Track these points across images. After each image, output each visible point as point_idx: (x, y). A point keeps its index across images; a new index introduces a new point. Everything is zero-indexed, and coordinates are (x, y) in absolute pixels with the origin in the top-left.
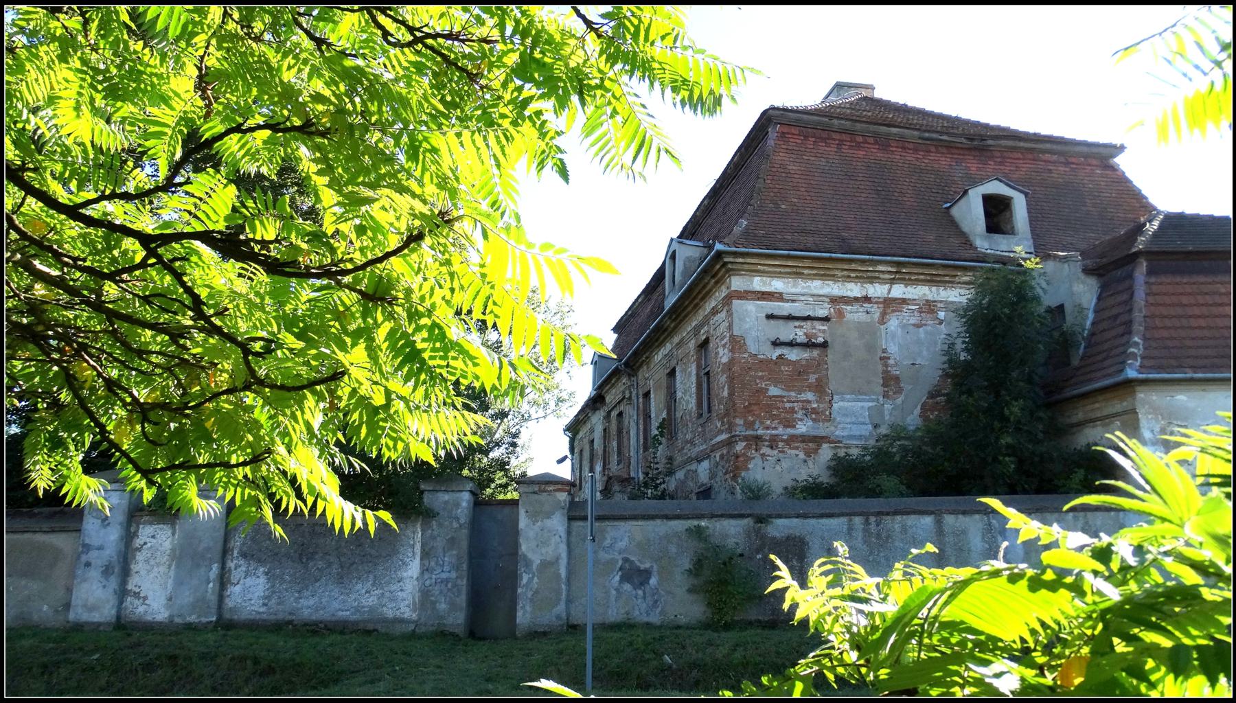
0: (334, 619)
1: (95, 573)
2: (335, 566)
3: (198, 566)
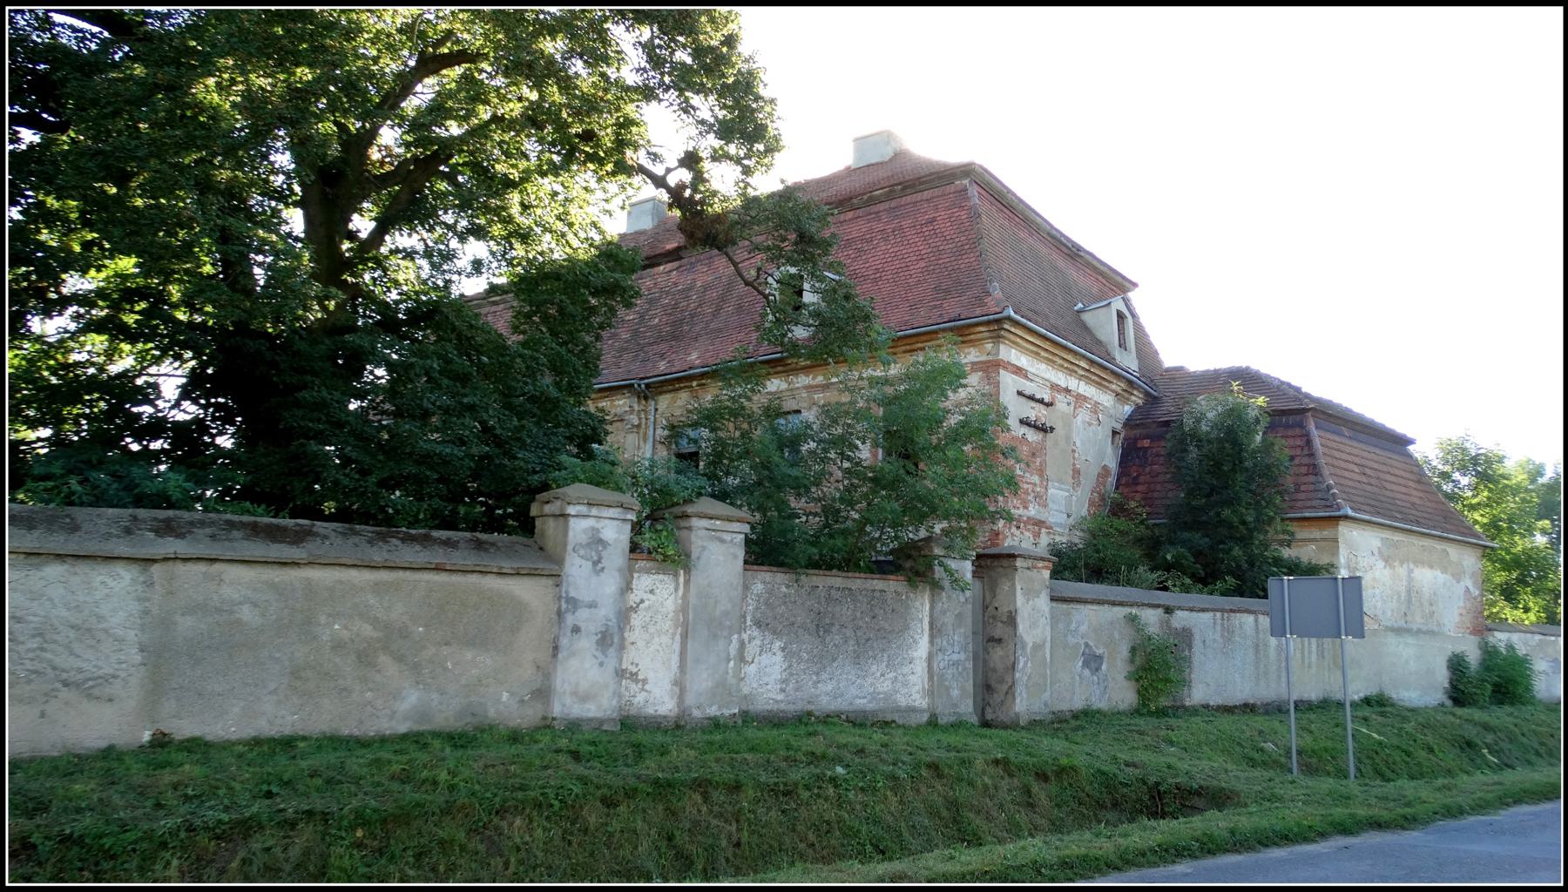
0: (851, 708)
1: (586, 643)
2: (852, 642)
3: (715, 636)
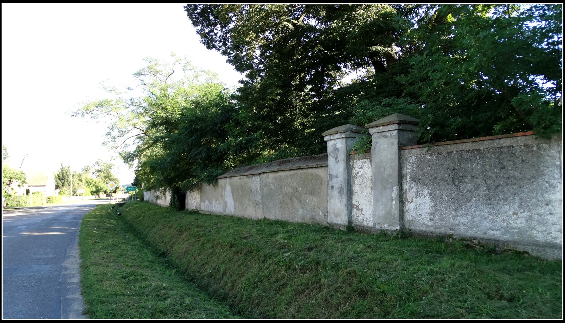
2: (483, 188)
